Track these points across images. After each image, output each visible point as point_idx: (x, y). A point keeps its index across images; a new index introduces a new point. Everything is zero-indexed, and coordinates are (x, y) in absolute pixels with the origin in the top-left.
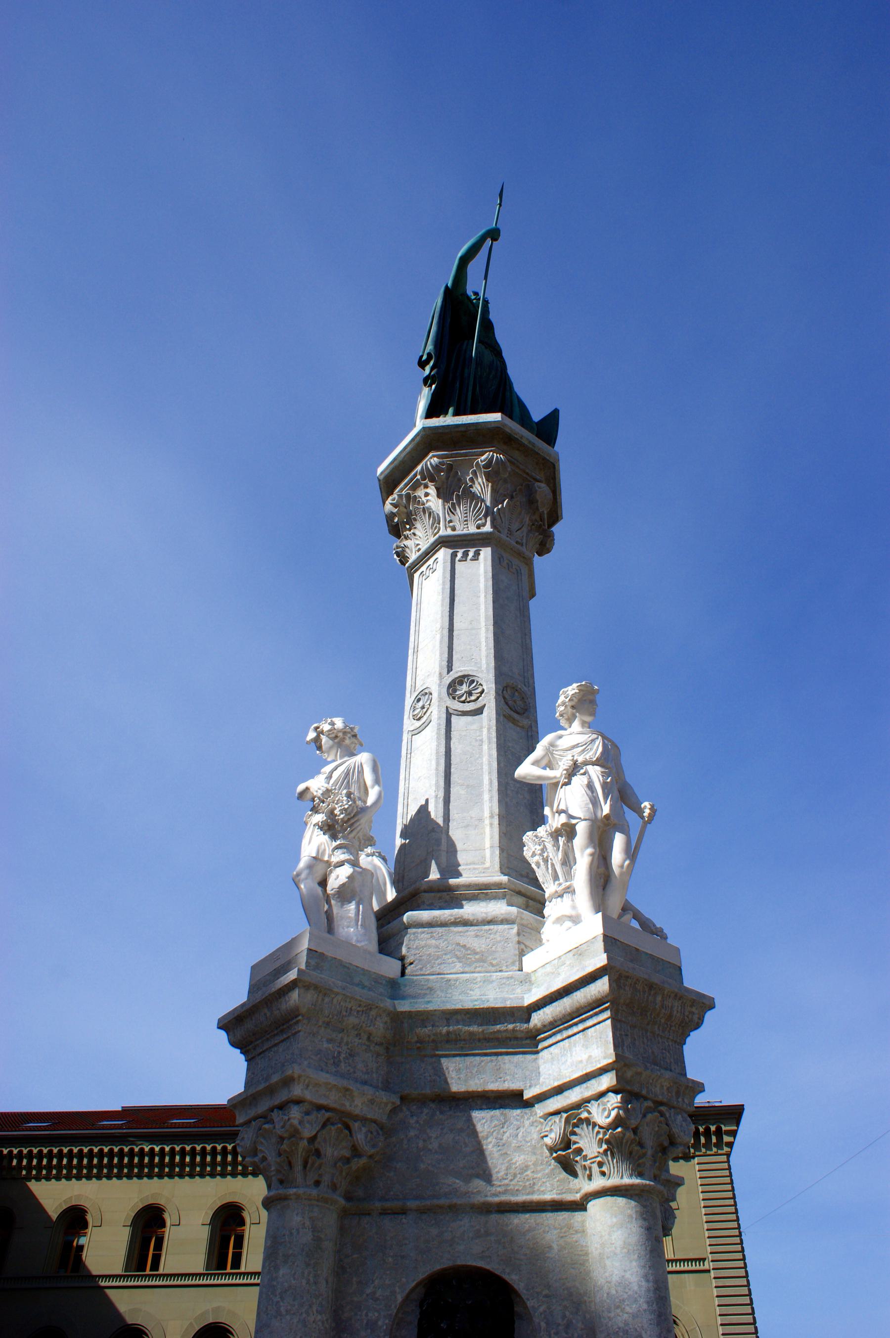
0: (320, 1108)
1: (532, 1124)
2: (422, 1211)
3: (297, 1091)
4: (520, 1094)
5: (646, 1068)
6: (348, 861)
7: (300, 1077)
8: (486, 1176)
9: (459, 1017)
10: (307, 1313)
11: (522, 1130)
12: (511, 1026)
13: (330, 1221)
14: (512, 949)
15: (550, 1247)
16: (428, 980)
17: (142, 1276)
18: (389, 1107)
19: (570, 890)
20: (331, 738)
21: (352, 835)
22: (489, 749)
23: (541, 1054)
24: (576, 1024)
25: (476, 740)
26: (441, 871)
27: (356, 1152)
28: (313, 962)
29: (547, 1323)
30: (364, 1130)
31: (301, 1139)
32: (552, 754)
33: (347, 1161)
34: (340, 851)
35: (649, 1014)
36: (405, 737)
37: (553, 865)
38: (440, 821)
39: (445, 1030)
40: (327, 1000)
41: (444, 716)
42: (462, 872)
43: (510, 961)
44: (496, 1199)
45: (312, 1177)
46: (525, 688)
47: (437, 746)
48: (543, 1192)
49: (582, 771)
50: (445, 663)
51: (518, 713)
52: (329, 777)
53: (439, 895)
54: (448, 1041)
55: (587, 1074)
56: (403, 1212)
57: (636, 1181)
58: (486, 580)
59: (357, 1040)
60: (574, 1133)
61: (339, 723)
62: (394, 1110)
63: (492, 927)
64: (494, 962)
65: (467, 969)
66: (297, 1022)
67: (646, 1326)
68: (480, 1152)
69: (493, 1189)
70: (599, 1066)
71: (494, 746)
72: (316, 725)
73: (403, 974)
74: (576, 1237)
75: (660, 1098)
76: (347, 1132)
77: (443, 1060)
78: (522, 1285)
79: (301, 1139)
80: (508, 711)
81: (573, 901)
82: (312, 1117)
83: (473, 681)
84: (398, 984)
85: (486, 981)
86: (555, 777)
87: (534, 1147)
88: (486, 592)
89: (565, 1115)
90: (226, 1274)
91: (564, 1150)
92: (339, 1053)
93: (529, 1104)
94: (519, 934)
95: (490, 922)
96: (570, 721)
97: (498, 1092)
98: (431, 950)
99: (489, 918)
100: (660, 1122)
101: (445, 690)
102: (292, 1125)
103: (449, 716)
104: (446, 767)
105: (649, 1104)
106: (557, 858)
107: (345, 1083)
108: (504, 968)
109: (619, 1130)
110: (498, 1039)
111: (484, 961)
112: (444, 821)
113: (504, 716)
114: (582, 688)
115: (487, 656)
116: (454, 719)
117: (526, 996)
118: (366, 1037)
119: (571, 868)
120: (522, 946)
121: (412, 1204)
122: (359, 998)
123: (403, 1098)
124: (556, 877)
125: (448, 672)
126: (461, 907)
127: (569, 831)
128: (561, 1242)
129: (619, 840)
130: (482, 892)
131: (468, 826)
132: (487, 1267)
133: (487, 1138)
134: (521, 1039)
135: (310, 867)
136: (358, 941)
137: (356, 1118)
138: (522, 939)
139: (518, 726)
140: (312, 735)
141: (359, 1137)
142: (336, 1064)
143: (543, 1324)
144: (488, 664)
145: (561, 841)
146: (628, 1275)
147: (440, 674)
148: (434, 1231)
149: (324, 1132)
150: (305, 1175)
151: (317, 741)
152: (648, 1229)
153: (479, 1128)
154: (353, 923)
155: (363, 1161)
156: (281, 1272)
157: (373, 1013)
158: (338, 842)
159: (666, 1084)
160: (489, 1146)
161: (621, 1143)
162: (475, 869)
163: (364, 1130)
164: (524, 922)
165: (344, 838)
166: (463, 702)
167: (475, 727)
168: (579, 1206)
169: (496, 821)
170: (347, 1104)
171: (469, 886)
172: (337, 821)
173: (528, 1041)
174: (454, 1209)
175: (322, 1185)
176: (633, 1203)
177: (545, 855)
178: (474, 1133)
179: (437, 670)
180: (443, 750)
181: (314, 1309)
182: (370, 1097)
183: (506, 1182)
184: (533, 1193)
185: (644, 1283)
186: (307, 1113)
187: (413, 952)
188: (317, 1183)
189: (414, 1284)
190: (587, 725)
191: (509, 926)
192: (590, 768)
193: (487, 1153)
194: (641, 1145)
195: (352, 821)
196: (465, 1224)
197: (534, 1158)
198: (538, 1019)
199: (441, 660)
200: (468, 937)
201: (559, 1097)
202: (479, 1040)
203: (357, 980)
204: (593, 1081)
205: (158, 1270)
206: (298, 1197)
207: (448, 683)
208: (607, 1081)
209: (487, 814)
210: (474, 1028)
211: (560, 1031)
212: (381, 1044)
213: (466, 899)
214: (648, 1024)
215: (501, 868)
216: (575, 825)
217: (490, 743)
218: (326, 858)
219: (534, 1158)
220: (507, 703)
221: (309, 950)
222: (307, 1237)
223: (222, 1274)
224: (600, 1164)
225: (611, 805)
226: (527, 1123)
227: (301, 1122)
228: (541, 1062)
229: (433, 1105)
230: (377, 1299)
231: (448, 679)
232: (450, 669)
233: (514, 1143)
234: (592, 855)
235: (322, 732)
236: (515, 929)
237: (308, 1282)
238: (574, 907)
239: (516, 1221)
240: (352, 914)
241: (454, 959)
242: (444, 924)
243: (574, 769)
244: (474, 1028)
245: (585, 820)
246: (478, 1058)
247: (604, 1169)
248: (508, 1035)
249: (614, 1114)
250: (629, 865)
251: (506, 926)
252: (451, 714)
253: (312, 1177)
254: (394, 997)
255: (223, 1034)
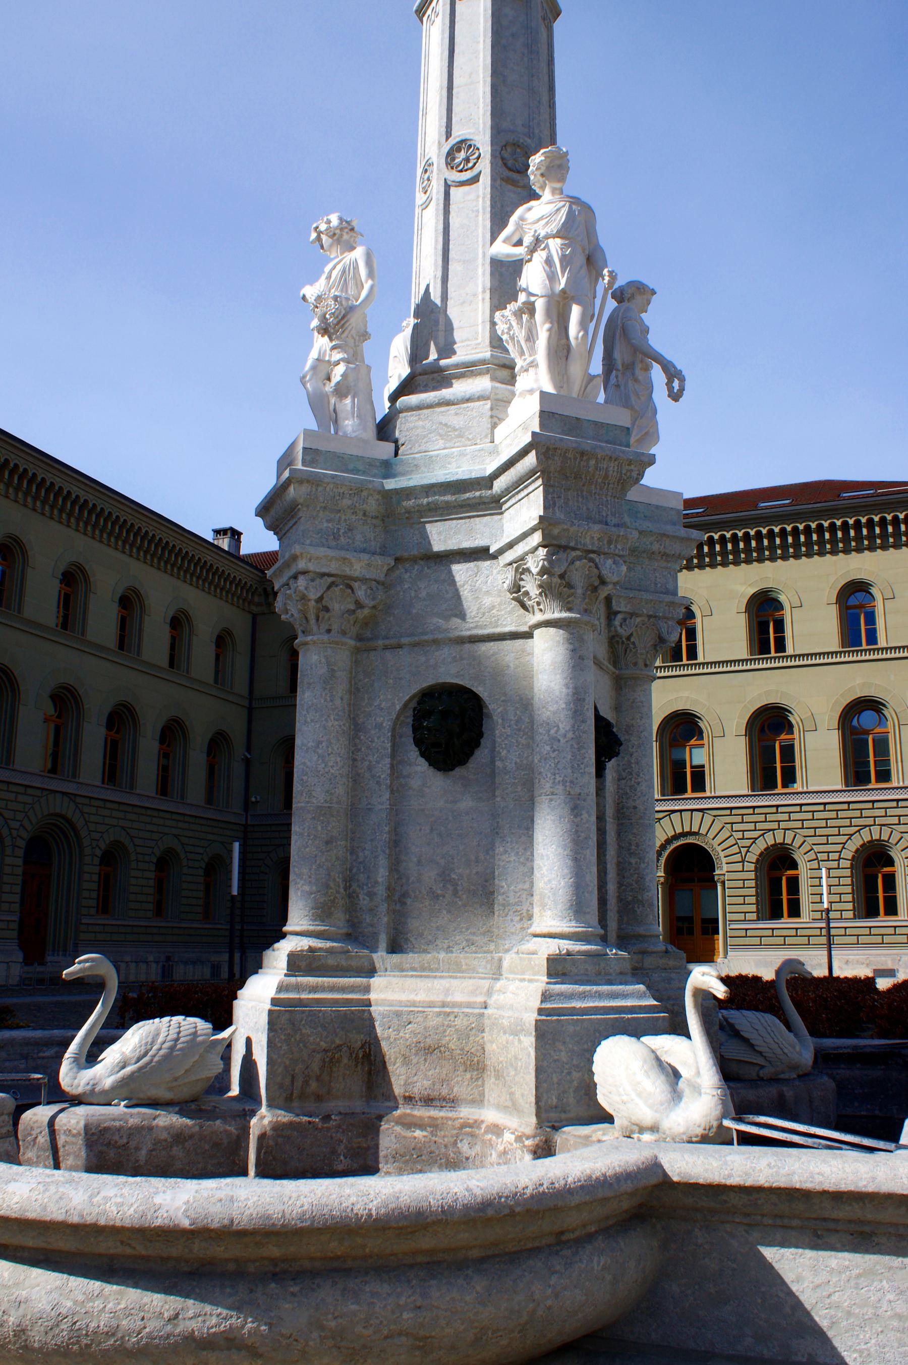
0: (323, 575)
1: (498, 573)
2: (414, 645)
3: (301, 565)
4: (486, 549)
5: (573, 524)
6: (342, 360)
7: (301, 554)
8: (462, 616)
9: (436, 489)
10: (326, 720)
11: (491, 577)
12: (477, 494)
13: (343, 658)
14: (486, 423)
15: (508, 666)
16: (414, 458)
17: (767, 659)
18: (386, 568)
19: (533, 364)
20: (330, 237)
21: (344, 336)
22: (483, 220)
23: (506, 514)
24: (522, 490)
25: (473, 211)
26: (439, 351)
27: (359, 605)
28: (308, 458)
29: (503, 719)
30: (364, 587)
31: (309, 600)
32: (522, 228)
33: (353, 612)
34: (336, 351)
35: (583, 476)
36: (417, 211)
37: (518, 341)
38: (438, 301)
39: (425, 501)
40: (320, 489)
41: (442, 189)
42: (457, 350)
43: (484, 434)
44: (468, 633)
45: (324, 627)
46: (529, 141)
47: (436, 223)
48: (505, 626)
49: (543, 246)
50: (444, 129)
51: (518, 172)
52: (329, 277)
53: (431, 376)
54: (430, 510)
55: (524, 533)
56: (400, 646)
57: (565, 615)
58: (485, 21)
59: (353, 517)
60: (522, 580)
61: (334, 220)
62: (391, 570)
63: (469, 404)
64: (470, 437)
65: (447, 445)
66: (299, 510)
67: (562, 719)
68: (457, 597)
69: (467, 626)
70: (530, 526)
71: (488, 216)
72: (315, 225)
73: (396, 454)
74: (527, 658)
75: (590, 547)
76: (349, 591)
77: (427, 526)
78: (486, 694)
79: (309, 600)
80: (507, 173)
81: (536, 374)
82: (318, 581)
83: (470, 146)
84: (391, 464)
85: (462, 454)
86: (521, 254)
87: (500, 591)
88: (485, 36)
89: (515, 565)
90: (771, 658)
91: (516, 593)
92: (338, 529)
93: (494, 557)
94: (492, 409)
95: (468, 400)
96: (543, 188)
97: (470, 548)
98: (419, 431)
99: (468, 397)
100: (590, 567)
101: (443, 161)
102: (300, 591)
103: (447, 187)
104: (444, 244)
105: (578, 553)
106: (521, 335)
107: (343, 553)
108: (478, 441)
109: (545, 577)
110: (469, 505)
111: (462, 437)
112: (442, 301)
113: (502, 179)
114: (547, 155)
115: (484, 115)
116: (453, 191)
117: (488, 467)
118: (362, 513)
119: (534, 343)
120: (496, 420)
121: (404, 640)
122: (348, 484)
123: (397, 560)
124: (522, 353)
125: (447, 139)
126: (450, 385)
127: (530, 308)
128: (517, 662)
129: (576, 311)
130: (469, 369)
131: (464, 302)
132: (461, 683)
133: (464, 585)
134: (489, 503)
135: (314, 368)
136: (354, 431)
137: (356, 579)
138: (495, 413)
139: (518, 187)
140: (314, 235)
141: (359, 593)
142: (336, 537)
143: (500, 721)
144: (484, 124)
145: (525, 317)
146: (552, 685)
147: (439, 142)
148: (423, 659)
149: (329, 593)
150: (319, 627)
151: (319, 238)
152: (573, 650)
153: (457, 578)
154: (350, 415)
155: (366, 611)
156: (306, 695)
157: (365, 493)
158: (334, 343)
159: (596, 536)
160: (465, 593)
161: (551, 587)
162: (468, 346)
163: (364, 587)
164: (499, 397)
165: (337, 338)
166: (461, 171)
167: (472, 196)
168: (528, 635)
169: (488, 295)
170: (347, 569)
171: (457, 366)
172: (329, 324)
173: (493, 505)
174: (436, 642)
175: (333, 632)
176: (561, 632)
177: (511, 333)
178: (453, 582)
179: (437, 138)
180: (441, 227)
181: (332, 718)
182: (367, 562)
183: (477, 619)
184: (497, 627)
185: (564, 690)
186: (313, 580)
187: (404, 434)
188: (329, 631)
189: (407, 698)
190: (557, 192)
191: (484, 402)
192: (551, 242)
193: (463, 598)
194: (569, 586)
195: (342, 322)
196: (446, 652)
197: (499, 600)
198: (499, 485)
199: (440, 126)
200: (449, 415)
201: (511, 551)
202: (455, 507)
203: (351, 466)
204: (529, 538)
205: (861, 646)
206: (315, 643)
207: (446, 151)
208: (537, 538)
209: (480, 289)
210: (448, 498)
211: (513, 496)
212: (377, 517)
213: (455, 378)
214: (584, 485)
215: (491, 342)
216: (534, 302)
217: (484, 213)
218: (327, 358)
219: (499, 600)
220: (505, 165)
221: (304, 448)
222: (323, 670)
223: (680, 666)
224: (538, 604)
225: (568, 278)
226: (495, 572)
227: (306, 588)
228: (504, 521)
229: (422, 563)
230: (382, 709)
231: (446, 148)
232: (448, 134)
233: (484, 589)
234: (550, 330)
235: (321, 232)
236: (488, 404)
237: (325, 700)
238: (537, 380)
239: (483, 648)
240: (349, 408)
241: (438, 437)
242: (430, 406)
243: (537, 242)
244: (448, 498)
245: (542, 297)
246: (454, 521)
247: (541, 607)
248: (477, 501)
249: (541, 564)
250: (583, 336)
251: (481, 403)
252: (450, 186)
253: (324, 627)
254: (387, 476)
255: (259, 520)
